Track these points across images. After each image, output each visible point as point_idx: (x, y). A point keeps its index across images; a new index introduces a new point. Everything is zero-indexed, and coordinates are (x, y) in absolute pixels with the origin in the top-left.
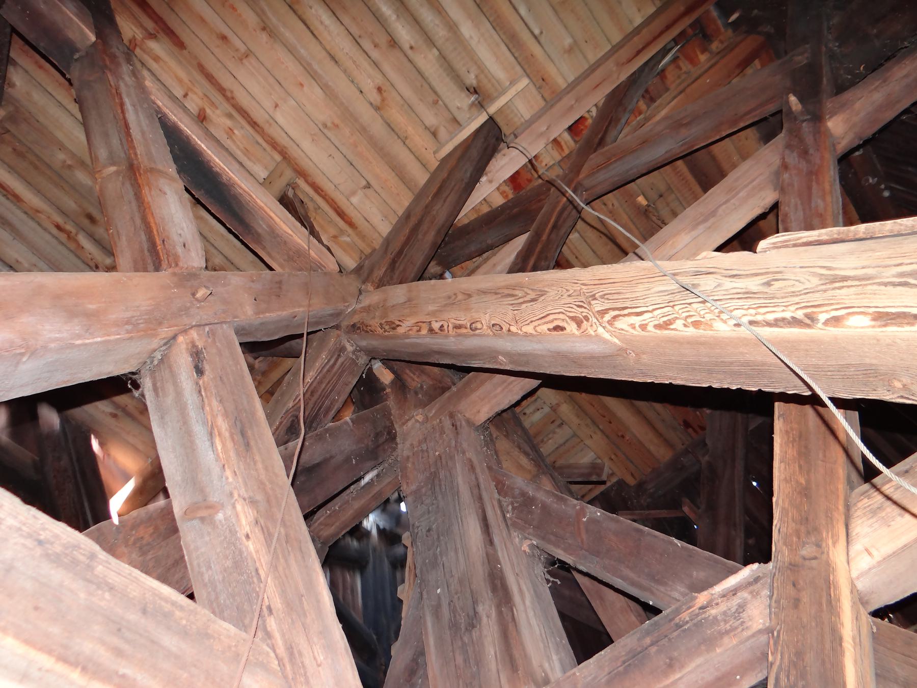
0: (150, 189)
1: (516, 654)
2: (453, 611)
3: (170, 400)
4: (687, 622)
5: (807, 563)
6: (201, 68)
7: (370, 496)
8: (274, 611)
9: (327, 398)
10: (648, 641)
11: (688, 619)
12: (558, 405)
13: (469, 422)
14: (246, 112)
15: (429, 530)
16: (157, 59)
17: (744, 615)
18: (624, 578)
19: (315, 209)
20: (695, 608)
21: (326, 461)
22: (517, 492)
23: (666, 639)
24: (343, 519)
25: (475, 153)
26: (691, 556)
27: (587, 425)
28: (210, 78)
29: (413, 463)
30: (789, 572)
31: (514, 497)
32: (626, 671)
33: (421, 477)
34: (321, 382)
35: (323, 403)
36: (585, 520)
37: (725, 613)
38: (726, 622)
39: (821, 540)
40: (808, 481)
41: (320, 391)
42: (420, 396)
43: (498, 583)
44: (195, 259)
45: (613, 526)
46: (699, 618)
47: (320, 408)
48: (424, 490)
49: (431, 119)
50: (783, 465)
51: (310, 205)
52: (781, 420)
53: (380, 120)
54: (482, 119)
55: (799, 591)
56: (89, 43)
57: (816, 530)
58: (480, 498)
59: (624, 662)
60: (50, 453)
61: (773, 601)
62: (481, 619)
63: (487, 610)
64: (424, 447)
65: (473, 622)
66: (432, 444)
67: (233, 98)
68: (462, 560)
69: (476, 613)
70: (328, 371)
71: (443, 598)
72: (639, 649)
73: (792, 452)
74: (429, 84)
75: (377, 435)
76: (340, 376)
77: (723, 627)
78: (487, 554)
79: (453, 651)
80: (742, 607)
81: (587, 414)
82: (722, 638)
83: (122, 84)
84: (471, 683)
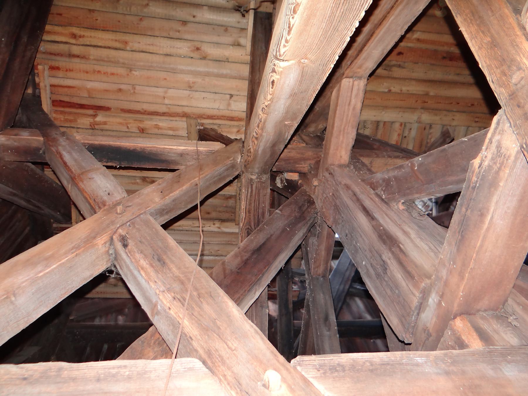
0: (83, 182)
1: (410, 269)
2: (375, 269)
3: (125, 269)
4: (477, 181)
5: (519, 86)
6: (124, 111)
7: (325, 238)
8: (193, 338)
9: (259, 208)
10: (464, 209)
11: (476, 179)
12: (419, 118)
13: (341, 166)
14: (155, 112)
15: (347, 235)
16: (105, 123)
17: (503, 150)
18: (451, 184)
19: (219, 127)
20: (477, 170)
21: (268, 240)
22: (381, 181)
23: (472, 201)
24: (323, 258)
25: (260, 36)
26: (476, 141)
27: (446, 115)
28: (130, 111)
29: (325, 208)
30: (512, 101)
31: (381, 185)
32: (463, 237)
33: (331, 212)
34: (250, 204)
35: (258, 212)
36: (416, 168)
37: (493, 159)
38: (495, 163)
39: (519, 64)
40: (492, 37)
41: (253, 209)
42: (312, 172)
43: (385, 237)
44: (119, 194)
45: (430, 160)
46: (481, 174)
47: (258, 216)
48: (337, 217)
49: (227, 39)
50: (473, 41)
51: (216, 127)
52: (458, 16)
53: (210, 62)
54: (251, 16)
55: (523, 107)
56: (42, 142)
57: (513, 60)
58: (358, 200)
59: (459, 232)
60: (95, 325)
61: (513, 127)
62: (387, 263)
63: (387, 256)
64: (325, 196)
65: (385, 267)
66: (327, 191)
67: (145, 111)
68: (365, 239)
69: (384, 261)
70: (251, 196)
71: (367, 265)
72: (462, 218)
73: (473, 29)
74: (216, 25)
75: (300, 208)
76: (259, 194)
77: (495, 168)
78: (373, 226)
79: (384, 290)
80: (499, 147)
81: (440, 110)
82: (499, 175)
83: (60, 148)
84: (399, 301)
